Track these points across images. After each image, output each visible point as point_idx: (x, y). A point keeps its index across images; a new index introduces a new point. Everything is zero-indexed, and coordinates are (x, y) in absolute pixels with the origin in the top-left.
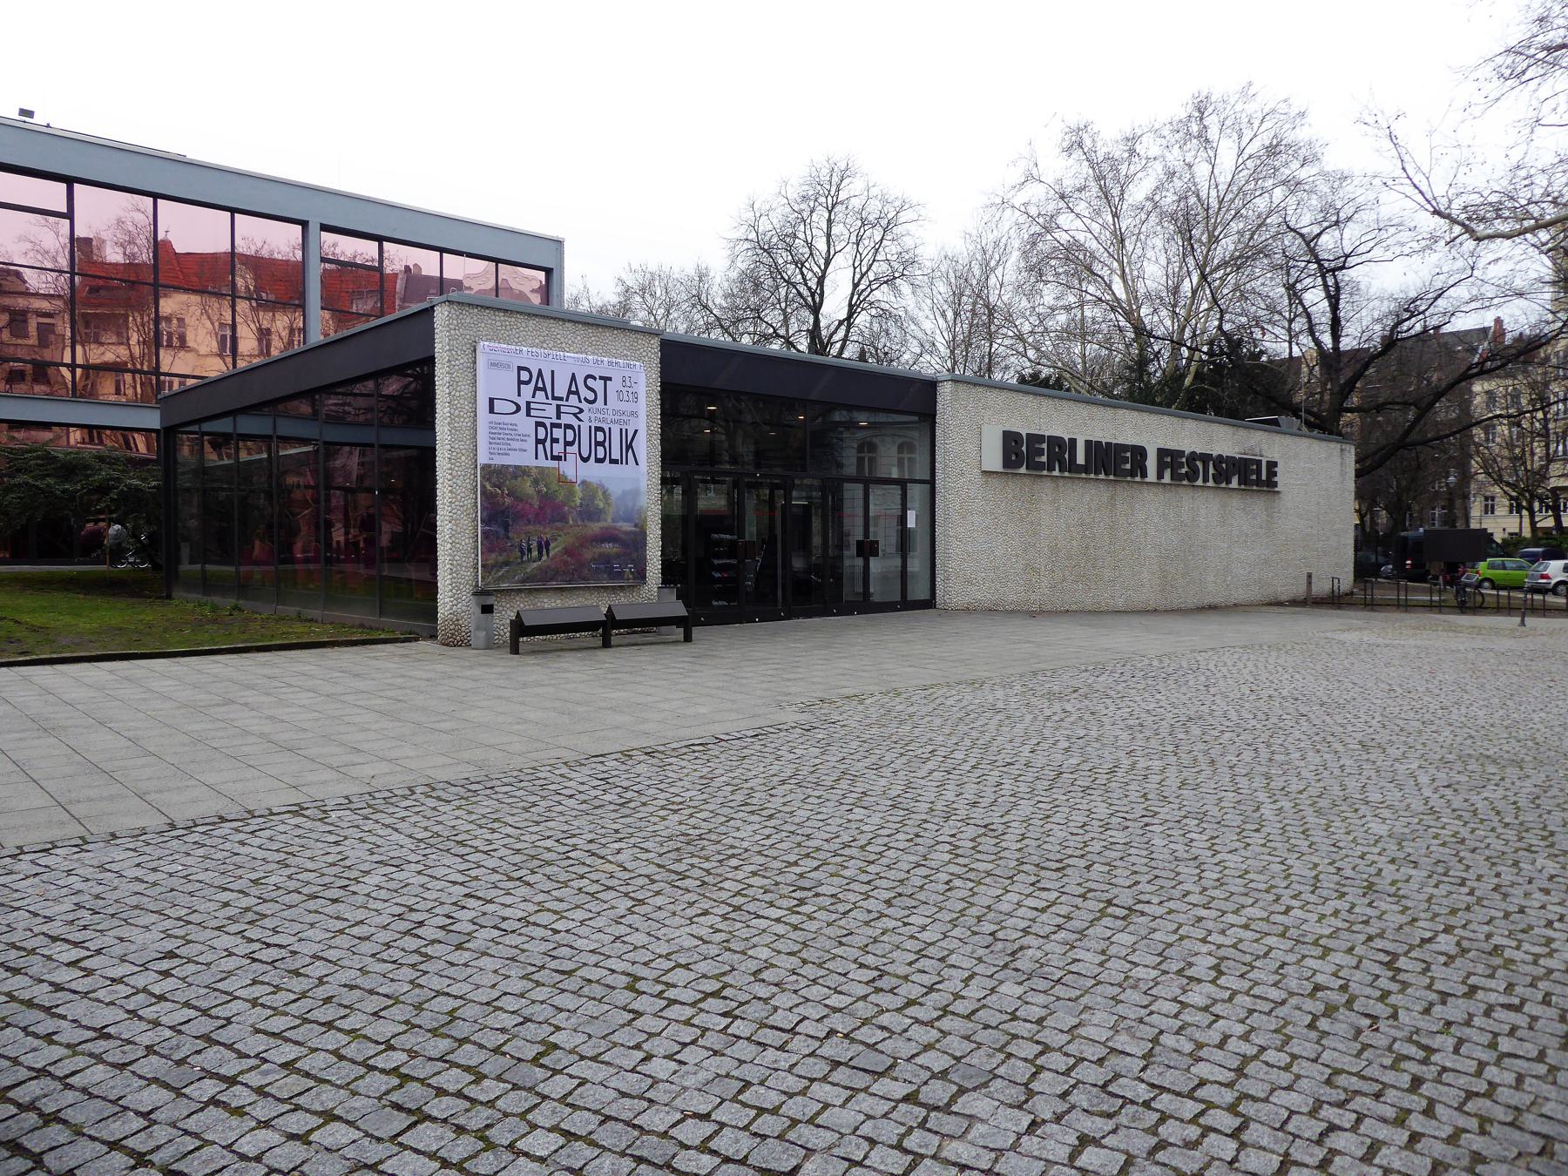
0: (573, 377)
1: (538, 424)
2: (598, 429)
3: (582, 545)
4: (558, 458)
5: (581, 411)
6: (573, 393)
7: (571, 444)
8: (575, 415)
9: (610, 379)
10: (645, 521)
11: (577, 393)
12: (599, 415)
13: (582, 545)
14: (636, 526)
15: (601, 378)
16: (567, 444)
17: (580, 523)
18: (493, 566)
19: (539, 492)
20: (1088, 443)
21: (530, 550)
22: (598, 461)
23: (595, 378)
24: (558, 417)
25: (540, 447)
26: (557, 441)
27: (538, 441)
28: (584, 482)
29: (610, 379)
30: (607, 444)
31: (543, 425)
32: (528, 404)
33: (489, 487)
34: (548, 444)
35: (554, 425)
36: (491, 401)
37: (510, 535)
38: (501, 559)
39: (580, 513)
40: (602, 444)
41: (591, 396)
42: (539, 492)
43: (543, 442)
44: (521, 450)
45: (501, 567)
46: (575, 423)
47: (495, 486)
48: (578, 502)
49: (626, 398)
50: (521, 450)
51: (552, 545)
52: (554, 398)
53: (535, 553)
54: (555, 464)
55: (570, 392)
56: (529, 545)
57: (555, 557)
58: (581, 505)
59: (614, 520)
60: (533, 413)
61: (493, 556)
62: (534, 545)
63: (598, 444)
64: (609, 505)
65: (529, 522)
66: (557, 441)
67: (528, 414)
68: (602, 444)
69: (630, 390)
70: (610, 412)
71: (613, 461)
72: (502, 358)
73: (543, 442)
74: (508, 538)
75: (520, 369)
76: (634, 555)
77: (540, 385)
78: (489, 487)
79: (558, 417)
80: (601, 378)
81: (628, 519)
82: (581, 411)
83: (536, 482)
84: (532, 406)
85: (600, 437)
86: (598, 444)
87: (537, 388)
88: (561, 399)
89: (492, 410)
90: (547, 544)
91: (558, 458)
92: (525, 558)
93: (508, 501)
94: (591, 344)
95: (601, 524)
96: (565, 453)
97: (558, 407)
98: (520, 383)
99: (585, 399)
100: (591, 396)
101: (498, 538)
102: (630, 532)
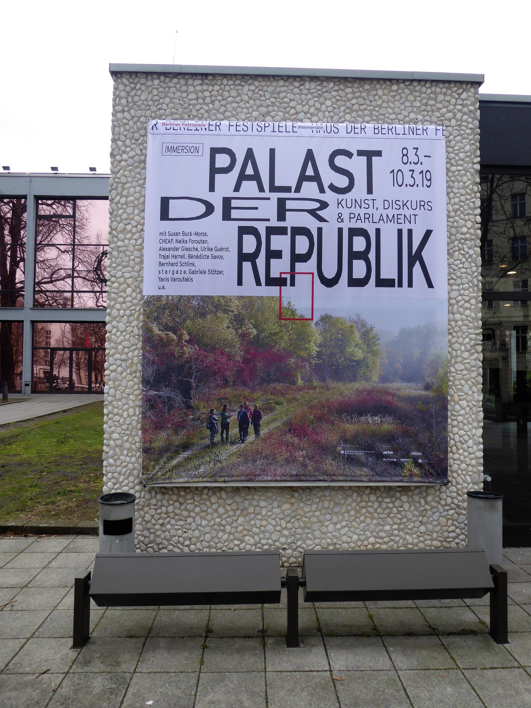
0: (310, 156)
1: (243, 231)
2: (354, 232)
3: (320, 419)
4: (280, 282)
5: (324, 205)
6: (310, 179)
7: (305, 258)
8: (312, 212)
9: (379, 153)
10: (445, 379)
11: (317, 178)
12: (357, 211)
13: (320, 419)
14: (427, 387)
15: (360, 153)
16: (296, 258)
17: (316, 383)
18: (162, 452)
19: (244, 336)
20: (286, 286)
21: (225, 426)
22: (353, 283)
23: (349, 155)
24: (281, 217)
25: (247, 266)
26: (278, 254)
27: (242, 257)
28: (326, 319)
29: (379, 153)
30: (372, 256)
31: (254, 231)
32: (227, 201)
33: (156, 330)
34: (261, 261)
35: (271, 231)
36: (165, 202)
37: (194, 402)
38: (177, 440)
39: (318, 369)
40: (363, 256)
41: (342, 182)
42: (244, 336)
43: (252, 258)
44: (213, 272)
45: (177, 453)
46: (312, 224)
47: (167, 328)
48: (314, 349)
49: (409, 180)
50: (213, 272)
51: (265, 418)
52: (273, 189)
53: (234, 431)
54: (274, 291)
55: (303, 178)
56: (224, 418)
57: (270, 435)
58: (319, 355)
59: (384, 379)
60: (234, 214)
61: (163, 435)
62: (233, 418)
63: (354, 255)
64: (374, 353)
65: (226, 383)
66: (278, 254)
67: (226, 216)
68: (363, 256)
69: (418, 168)
70: (379, 204)
71: (381, 283)
72: (187, 139)
73: (252, 258)
74: (189, 407)
75: (214, 151)
76: (423, 437)
77: (250, 171)
78: (156, 330)
79: (281, 217)
80: (360, 153)
81: (408, 378)
82: (324, 205)
83: (238, 320)
84: (234, 203)
85: (359, 244)
86: (354, 255)
87: (242, 177)
88: (288, 189)
89: (165, 215)
90: (257, 416)
91: (280, 282)
92: (217, 438)
93: (189, 350)
94: (351, 110)
95: (359, 385)
96: (293, 272)
97: (281, 202)
98: (214, 171)
99: (332, 187)
100: (342, 182)
101: (171, 407)
102: (420, 398)
